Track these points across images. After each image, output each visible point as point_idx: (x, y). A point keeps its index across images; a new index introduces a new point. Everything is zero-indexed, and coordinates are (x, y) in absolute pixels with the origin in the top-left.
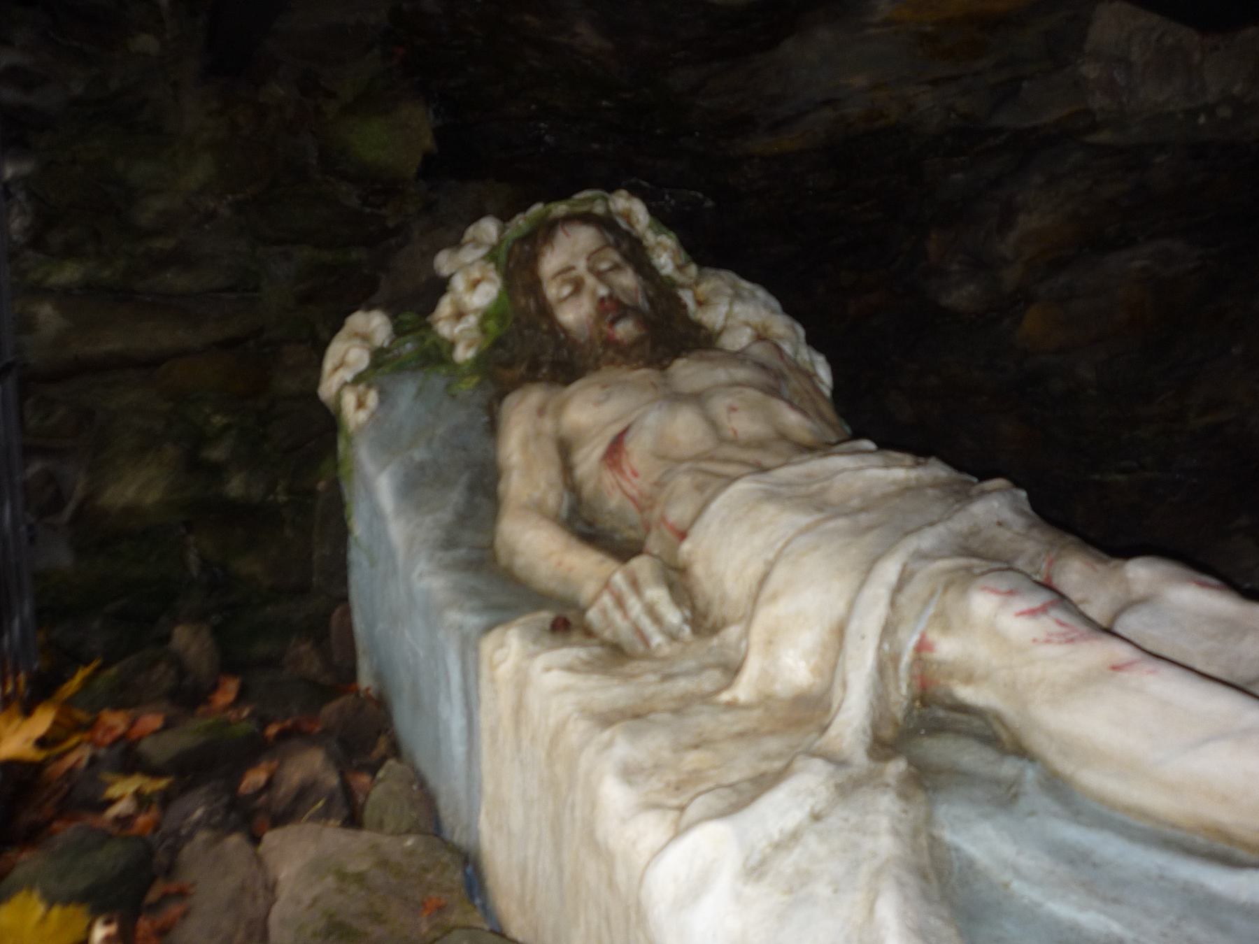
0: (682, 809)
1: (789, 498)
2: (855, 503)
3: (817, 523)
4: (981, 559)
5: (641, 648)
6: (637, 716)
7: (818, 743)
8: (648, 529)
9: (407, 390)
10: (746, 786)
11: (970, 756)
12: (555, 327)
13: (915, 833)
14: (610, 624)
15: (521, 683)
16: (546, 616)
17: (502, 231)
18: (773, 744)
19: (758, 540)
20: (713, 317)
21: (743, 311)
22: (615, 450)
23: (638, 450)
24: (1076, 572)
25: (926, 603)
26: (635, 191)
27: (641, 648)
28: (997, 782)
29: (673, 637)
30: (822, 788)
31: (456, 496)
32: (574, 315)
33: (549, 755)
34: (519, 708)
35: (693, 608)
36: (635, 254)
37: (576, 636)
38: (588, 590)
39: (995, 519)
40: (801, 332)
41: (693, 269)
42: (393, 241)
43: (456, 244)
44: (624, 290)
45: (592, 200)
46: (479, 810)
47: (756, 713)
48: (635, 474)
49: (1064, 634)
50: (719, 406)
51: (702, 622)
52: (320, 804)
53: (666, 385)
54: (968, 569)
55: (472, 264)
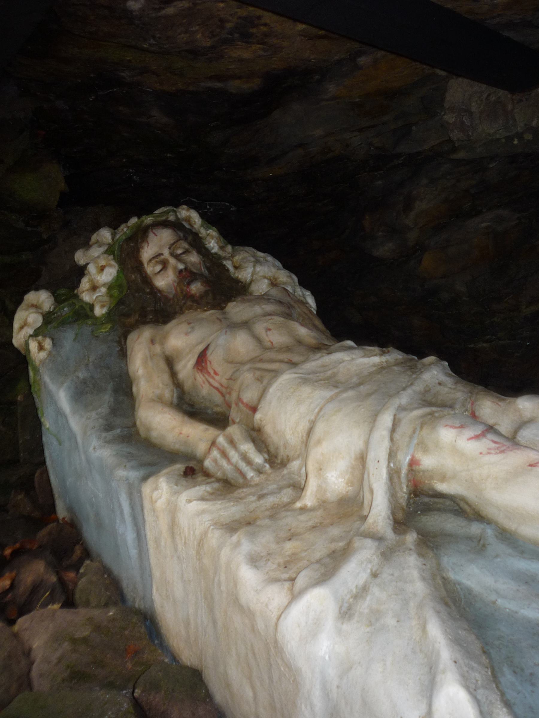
0: (292, 580)
1: (317, 381)
2: (355, 380)
3: (337, 395)
4: (434, 407)
5: (241, 481)
6: (249, 524)
7: (362, 528)
8: (229, 406)
9: (68, 337)
10: (327, 560)
11: (451, 524)
12: (154, 291)
13: (433, 577)
14: (220, 467)
15: (173, 511)
16: (180, 467)
17: (113, 235)
18: (335, 531)
19: (303, 409)
20: (245, 275)
21: (262, 270)
22: (202, 360)
23: (216, 359)
24: (489, 407)
25: (411, 437)
26: (192, 206)
27: (241, 481)
28: (470, 538)
29: (259, 471)
30: (374, 557)
31: (107, 398)
32: (164, 282)
33: (198, 553)
34: (173, 525)
35: (268, 452)
36: (197, 243)
37: (200, 478)
38: (201, 448)
39: (437, 381)
40: (296, 279)
41: (229, 248)
42: (47, 246)
43: (86, 245)
44: (193, 264)
45: (167, 213)
46: (152, 586)
47: (320, 513)
48: (216, 373)
49: (498, 448)
50: (260, 328)
51: (275, 460)
52: (48, 594)
53: (226, 318)
54: (431, 414)
55: (98, 257)
